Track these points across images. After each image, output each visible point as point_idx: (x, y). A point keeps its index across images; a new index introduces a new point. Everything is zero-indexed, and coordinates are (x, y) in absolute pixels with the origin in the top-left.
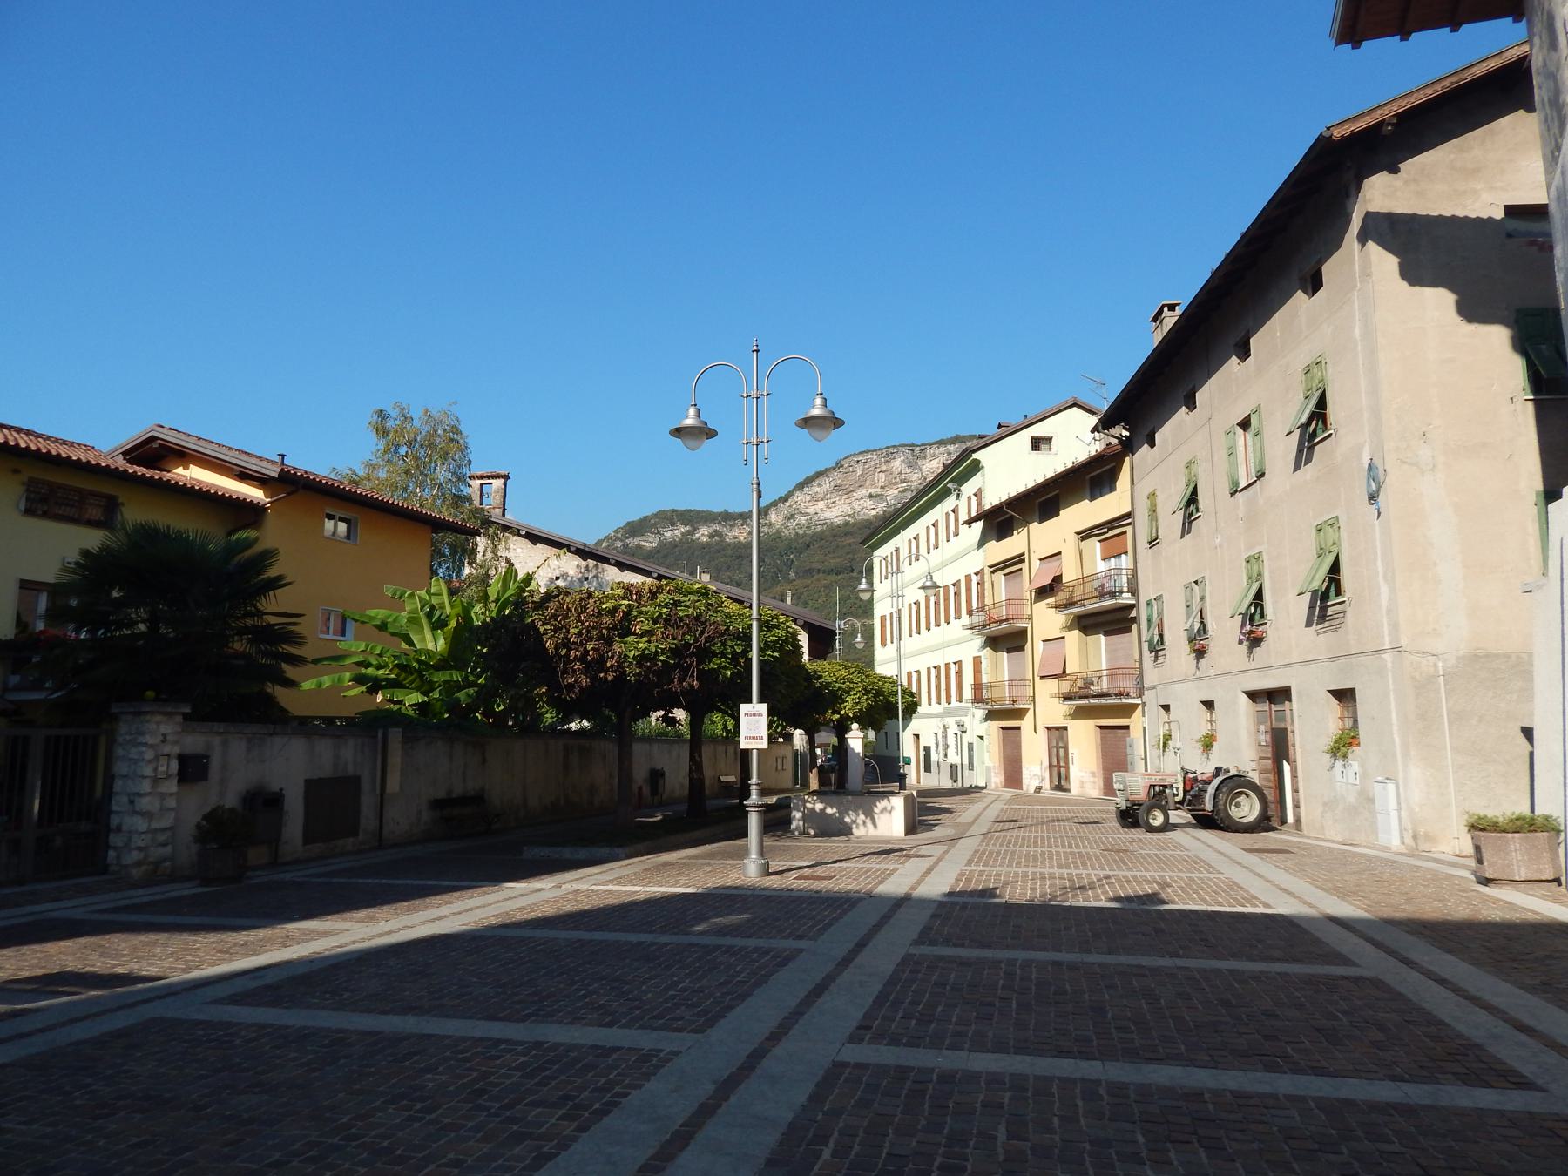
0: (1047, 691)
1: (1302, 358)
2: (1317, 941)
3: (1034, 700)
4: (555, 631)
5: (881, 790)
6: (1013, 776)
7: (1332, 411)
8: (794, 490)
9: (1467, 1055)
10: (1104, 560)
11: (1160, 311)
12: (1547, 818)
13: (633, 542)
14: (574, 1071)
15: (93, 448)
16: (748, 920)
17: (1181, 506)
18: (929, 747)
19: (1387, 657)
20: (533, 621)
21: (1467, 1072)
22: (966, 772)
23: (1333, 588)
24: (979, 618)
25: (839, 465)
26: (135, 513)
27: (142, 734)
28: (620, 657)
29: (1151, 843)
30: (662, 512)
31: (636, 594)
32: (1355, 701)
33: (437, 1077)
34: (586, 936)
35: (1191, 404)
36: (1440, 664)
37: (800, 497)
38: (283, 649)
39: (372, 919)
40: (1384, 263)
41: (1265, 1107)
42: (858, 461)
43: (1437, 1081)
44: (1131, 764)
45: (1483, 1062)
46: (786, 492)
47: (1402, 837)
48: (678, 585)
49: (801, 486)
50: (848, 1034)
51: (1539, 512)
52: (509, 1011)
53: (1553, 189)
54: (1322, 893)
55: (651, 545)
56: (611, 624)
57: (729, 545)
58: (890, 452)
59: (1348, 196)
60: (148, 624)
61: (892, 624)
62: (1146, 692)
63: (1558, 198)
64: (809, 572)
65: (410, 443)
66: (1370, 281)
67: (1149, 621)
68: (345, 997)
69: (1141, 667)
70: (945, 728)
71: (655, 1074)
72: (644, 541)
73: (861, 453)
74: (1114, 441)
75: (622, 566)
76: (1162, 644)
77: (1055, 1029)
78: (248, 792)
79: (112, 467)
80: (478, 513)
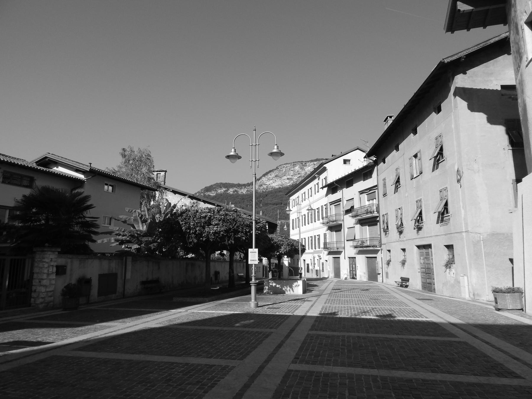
0: (349, 245)
1: (435, 134)
2: (444, 330)
3: (344, 248)
4: (185, 224)
5: (294, 278)
6: (337, 273)
7: (445, 152)
8: (262, 176)
9: (498, 367)
10: (368, 201)
11: (387, 118)
12: (518, 288)
13: (207, 194)
14: (200, 373)
15: (25, 160)
16: (253, 322)
17: (394, 183)
18: (309, 264)
19: (464, 234)
20: (178, 220)
21: (498, 373)
22: (321, 273)
23: (445, 211)
24: (325, 220)
25: (277, 168)
26: (40, 183)
27: (44, 258)
28: (207, 232)
29: (386, 297)
30: (217, 183)
31: (213, 211)
32: (453, 249)
33: (154, 375)
34: (199, 328)
35: (397, 149)
36: (481, 237)
37: (264, 179)
38: (92, 229)
39: (124, 322)
40: (462, 104)
41: (433, 384)
42: (284, 167)
43: (489, 376)
44: (377, 270)
45: (504, 370)
46: (259, 177)
47: (469, 295)
48: (227, 208)
49: (264, 175)
50: (291, 360)
51: (513, 186)
52: (175, 353)
53: (518, 80)
54: (444, 314)
55: (213, 195)
56: (204, 221)
57: (240, 195)
58: (294, 164)
59: (449, 81)
60: (45, 221)
61: (296, 222)
62: (382, 246)
63: (519, 84)
64: (267, 204)
65: (134, 159)
66: (457, 109)
67: (383, 222)
68: (118, 348)
69: (381, 238)
70: (314, 258)
71: (228, 374)
72: (211, 193)
73: (285, 164)
74: (371, 161)
75: (205, 202)
76: (388, 229)
77: (361, 359)
78: (79, 278)
79: (33, 167)
80: (156, 183)
